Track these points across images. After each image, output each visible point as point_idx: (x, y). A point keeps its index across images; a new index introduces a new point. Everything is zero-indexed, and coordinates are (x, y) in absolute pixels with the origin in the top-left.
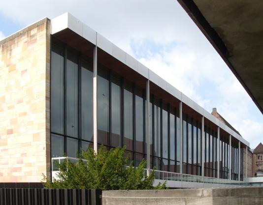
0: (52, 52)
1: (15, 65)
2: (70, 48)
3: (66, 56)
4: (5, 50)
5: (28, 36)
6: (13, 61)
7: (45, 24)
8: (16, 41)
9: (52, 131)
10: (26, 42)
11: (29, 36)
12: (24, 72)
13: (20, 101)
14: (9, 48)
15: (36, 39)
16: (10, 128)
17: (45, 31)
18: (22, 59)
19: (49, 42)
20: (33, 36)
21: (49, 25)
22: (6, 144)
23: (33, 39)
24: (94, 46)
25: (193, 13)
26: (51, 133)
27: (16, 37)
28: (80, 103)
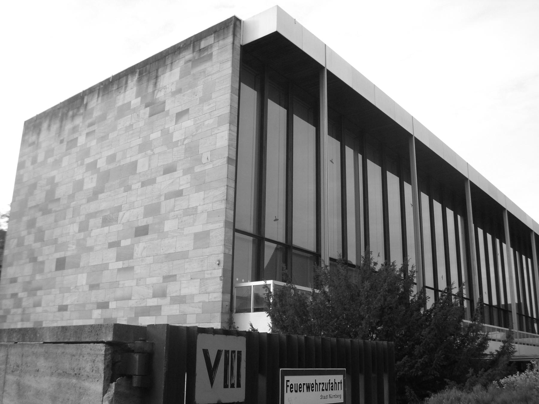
0: (242, 84)
1: (164, 102)
2: (278, 70)
3: (266, 93)
4: (145, 79)
5: (193, 52)
6: (160, 95)
7: (232, 26)
8: (168, 62)
9: (237, 227)
10: (190, 61)
11: (197, 49)
12: (180, 115)
13: (169, 170)
14: (154, 74)
15: (212, 53)
16: (142, 222)
17: (230, 39)
18: (179, 91)
19: (238, 57)
20: (206, 49)
21: (237, 29)
22: (130, 256)
23: (205, 54)
24: (321, 68)
25: (435, 392)
26: (235, 230)
27: (169, 54)
28: (289, 202)
